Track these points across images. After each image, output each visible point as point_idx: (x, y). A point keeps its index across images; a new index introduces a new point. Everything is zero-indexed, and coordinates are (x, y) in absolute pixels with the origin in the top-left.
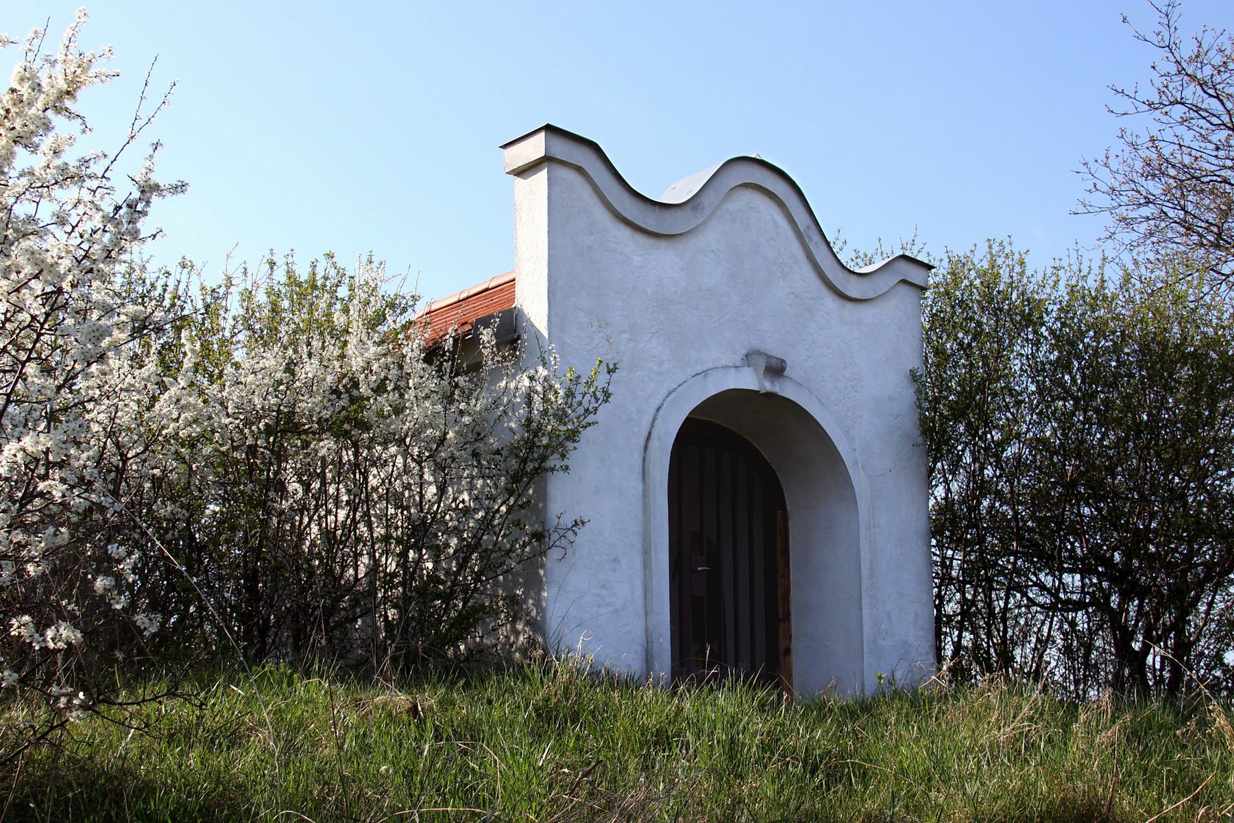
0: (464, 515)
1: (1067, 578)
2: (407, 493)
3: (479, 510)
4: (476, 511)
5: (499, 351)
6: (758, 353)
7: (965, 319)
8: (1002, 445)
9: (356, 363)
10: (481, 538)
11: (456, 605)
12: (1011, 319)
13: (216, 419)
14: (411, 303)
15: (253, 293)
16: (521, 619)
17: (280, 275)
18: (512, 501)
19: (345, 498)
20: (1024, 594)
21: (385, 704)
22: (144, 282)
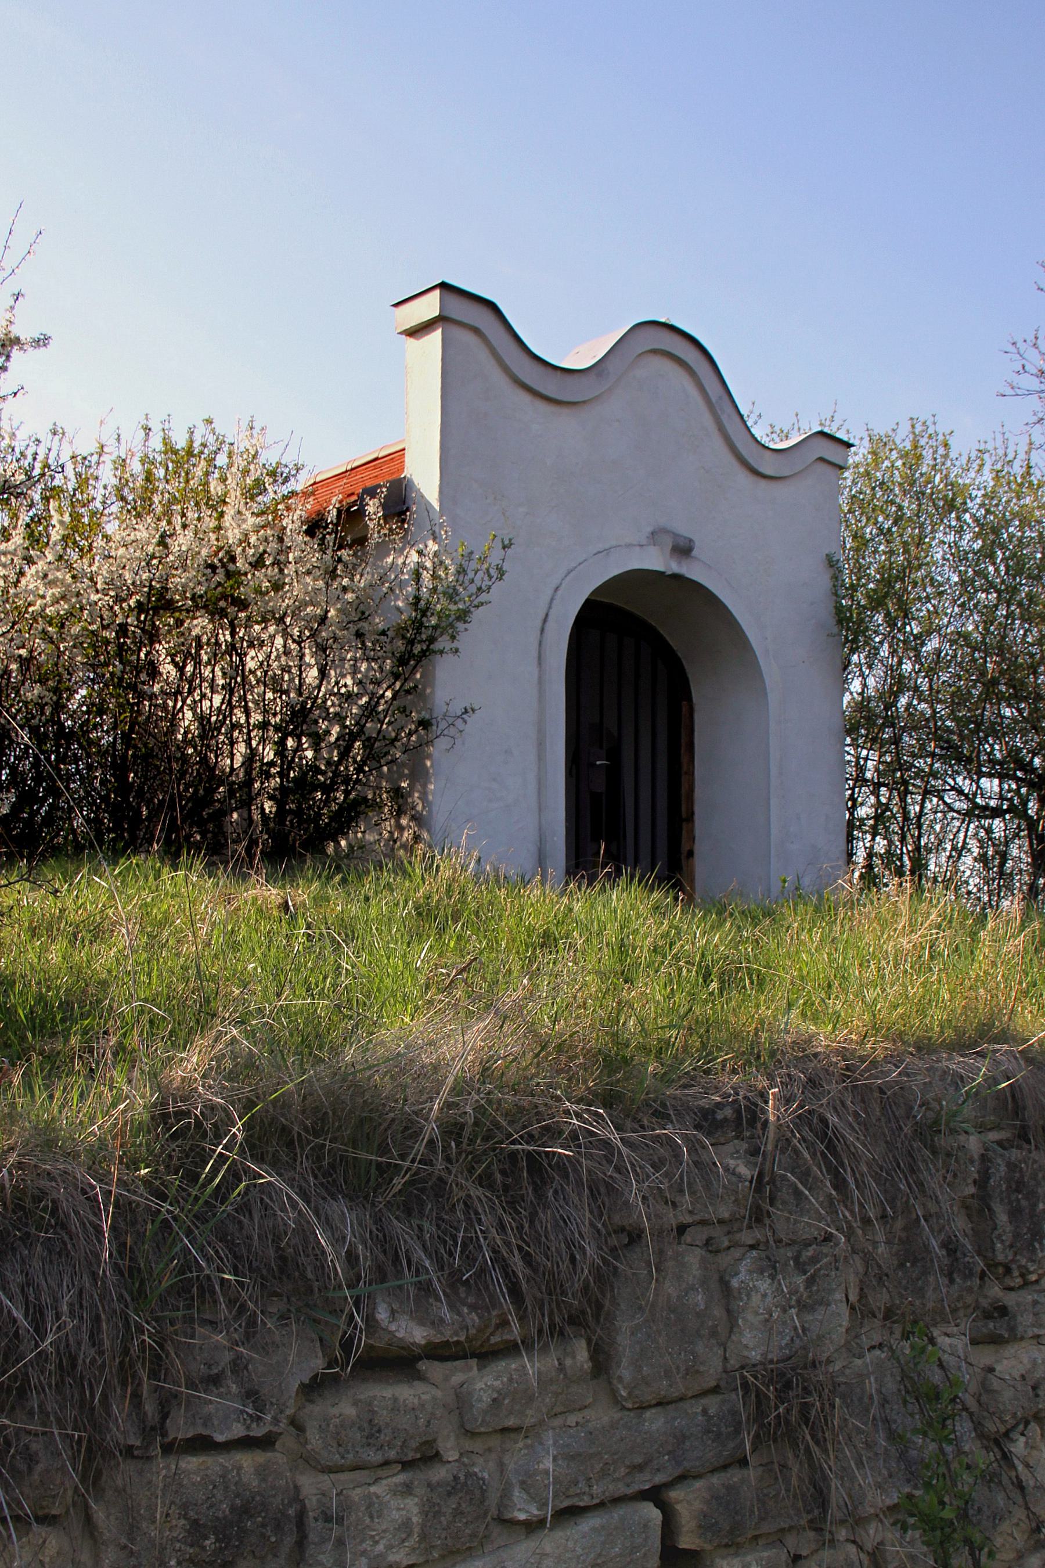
0: (346, 700)
1: (984, 782)
2: (286, 677)
3: (362, 695)
4: (359, 696)
5: (386, 523)
6: (664, 531)
7: (887, 502)
8: (921, 639)
9: (233, 535)
10: (364, 725)
11: (336, 798)
12: (934, 505)
13: (86, 595)
14: (293, 472)
15: (128, 461)
16: (406, 813)
17: (156, 443)
18: (398, 685)
19: (221, 682)
20: (941, 798)
21: (255, 899)
22: (13, 450)
